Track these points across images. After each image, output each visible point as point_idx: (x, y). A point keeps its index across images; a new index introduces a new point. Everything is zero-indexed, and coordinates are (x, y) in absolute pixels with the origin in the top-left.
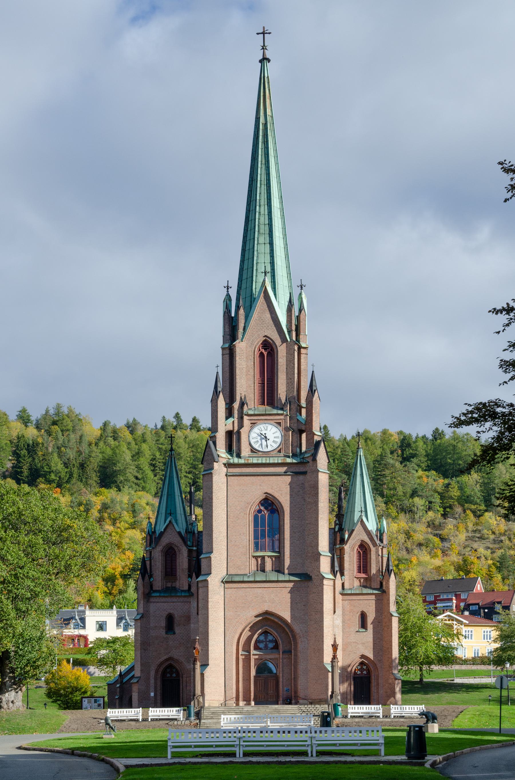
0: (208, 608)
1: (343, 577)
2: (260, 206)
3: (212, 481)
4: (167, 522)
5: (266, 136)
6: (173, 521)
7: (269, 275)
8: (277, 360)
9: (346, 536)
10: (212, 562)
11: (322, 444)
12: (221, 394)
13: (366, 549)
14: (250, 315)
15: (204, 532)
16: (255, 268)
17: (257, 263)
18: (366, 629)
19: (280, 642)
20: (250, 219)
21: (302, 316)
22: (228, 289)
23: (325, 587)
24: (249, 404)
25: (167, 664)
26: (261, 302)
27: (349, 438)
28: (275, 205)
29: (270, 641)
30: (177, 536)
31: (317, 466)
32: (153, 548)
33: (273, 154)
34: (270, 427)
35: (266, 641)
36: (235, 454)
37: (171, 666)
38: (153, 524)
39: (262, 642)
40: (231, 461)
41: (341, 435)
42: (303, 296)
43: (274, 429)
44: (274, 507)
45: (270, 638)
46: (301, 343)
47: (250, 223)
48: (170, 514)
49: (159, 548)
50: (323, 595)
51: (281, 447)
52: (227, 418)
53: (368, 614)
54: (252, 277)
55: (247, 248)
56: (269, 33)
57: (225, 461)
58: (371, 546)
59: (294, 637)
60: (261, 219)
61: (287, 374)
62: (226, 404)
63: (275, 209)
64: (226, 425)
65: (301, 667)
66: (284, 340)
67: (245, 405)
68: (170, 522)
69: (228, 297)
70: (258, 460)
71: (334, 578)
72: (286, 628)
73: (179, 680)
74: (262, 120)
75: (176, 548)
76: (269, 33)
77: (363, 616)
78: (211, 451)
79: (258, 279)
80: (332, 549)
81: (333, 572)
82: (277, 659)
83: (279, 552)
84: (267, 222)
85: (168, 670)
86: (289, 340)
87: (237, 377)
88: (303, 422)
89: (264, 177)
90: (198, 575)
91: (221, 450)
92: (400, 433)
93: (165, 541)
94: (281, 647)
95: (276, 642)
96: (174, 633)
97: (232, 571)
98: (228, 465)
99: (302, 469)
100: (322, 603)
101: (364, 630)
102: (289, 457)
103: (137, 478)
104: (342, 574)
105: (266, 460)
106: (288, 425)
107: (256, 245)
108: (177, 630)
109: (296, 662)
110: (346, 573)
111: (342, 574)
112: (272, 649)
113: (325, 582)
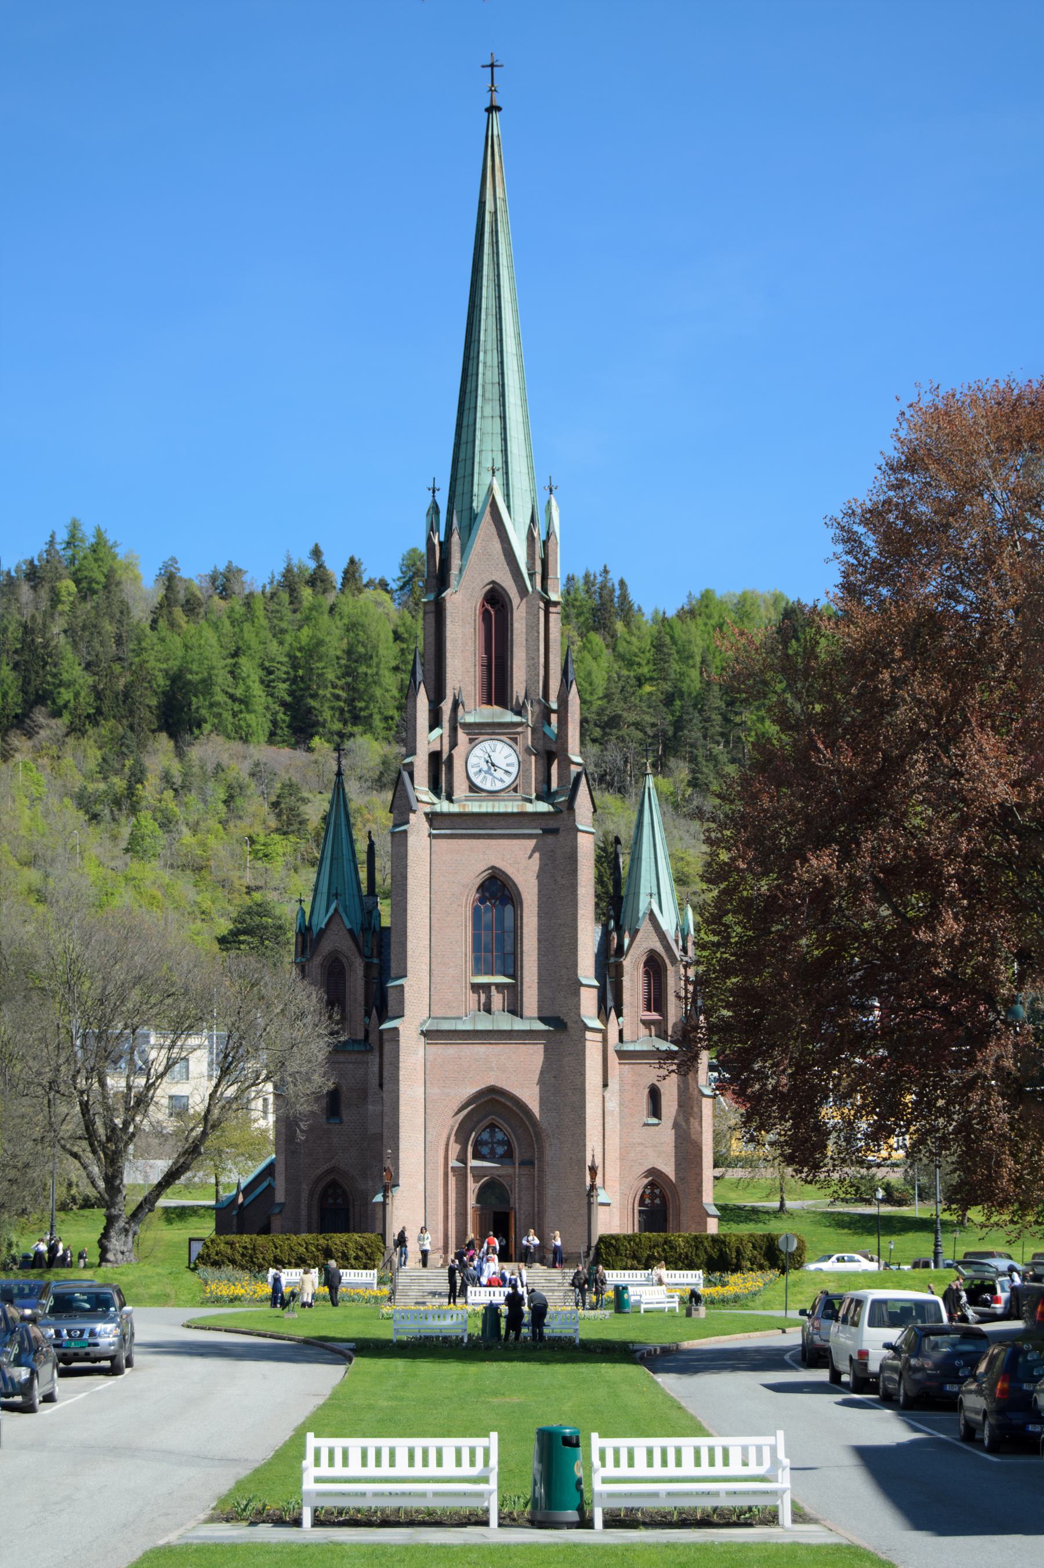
0: (398, 1080)
1: (621, 1019)
2: (485, 352)
3: (406, 845)
4: (331, 911)
5: (495, 232)
6: (341, 910)
7: (499, 474)
8: (512, 625)
9: (627, 941)
10: (406, 995)
11: (583, 780)
12: (422, 686)
13: (659, 966)
14: (469, 544)
15: (393, 931)
16: (477, 460)
17: (481, 451)
18: (660, 1118)
19: (515, 1144)
20: (470, 373)
21: (550, 544)
22: (434, 492)
23: (588, 1044)
24: (466, 703)
25: (329, 1178)
26: (486, 521)
27: (671, 613)
28: (509, 350)
29: (500, 1143)
30: (348, 937)
31: (574, 820)
32: (308, 960)
33: (505, 263)
34: (500, 745)
35: (493, 1143)
36: (444, 794)
37: (334, 1184)
38: (308, 910)
39: (486, 1143)
40: (438, 808)
41: (656, 612)
42: (554, 503)
43: (508, 750)
44: (506, 892)
45: (499, 1136)
46: (550, 593)
47: (469, 379)
48: (336, 895)
49: (317, 960)
50: (584, 1059)
51: (517, 782)
52: (431, 728)
53: (662, 1090)
54: (473, 474)
55: (465, 423)
56: (501, 66)
57: (428, 809)
58: (667, 961)
59: (538, 1134)
60: (486, 374)
61: (527, 649)
62: (430, 701)
63: (509, 355)
64: (429, 743)
65: (550, 1191)
66: (523, 592)
67: (461, 707)
68: (336, 910)
69: (435, 509)
70: (480, 806)
71: (603, 1027)
72: (524, 1118)
73: (348, 1209)
74: (489, 206)
75: (344, 960)
76: (501, 66)
77: (654, 1095)
78: (405, 790)
79: (484, 480)
80: (600, 975)
81: (603, 1013)
82: (509, 1176)
83: (513, 976)
84: (496, 380)
85: (330, 1191)
86: (530, 589)
87: (448, 655)
88: (553, 738)
89: (492, 302)
90: (383, 1017)
91: (421, 791)
92: (777, 599)
93: (326, 946)
94: (517, 1154)
95: (508, 1143)
96: (341, 1122)
97: (437, 1012)
98: (433, 818)
99: (552, 824)
100: (583, 1074)
101: (655, 1121)
102: (530, 801)
103: (232, 697)
104: (619, 1014)
105: (494, 807)
106: (530, 743)
107: (478, 420)
108: (346, 1114)
109: (541, 1182)
110: (625, 1011)
111: (619, 1014)
112: (502, 1157)
113: (589, 1035)
